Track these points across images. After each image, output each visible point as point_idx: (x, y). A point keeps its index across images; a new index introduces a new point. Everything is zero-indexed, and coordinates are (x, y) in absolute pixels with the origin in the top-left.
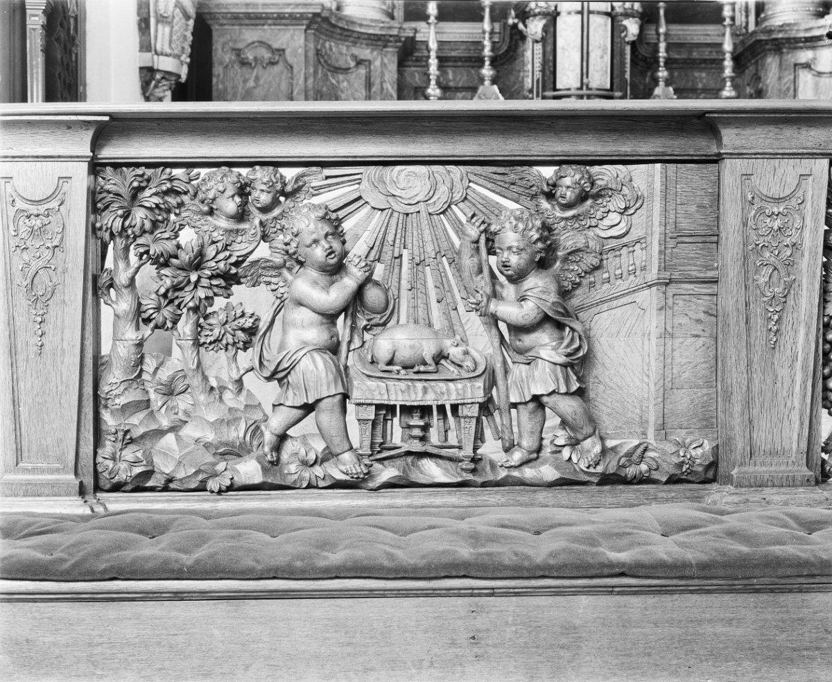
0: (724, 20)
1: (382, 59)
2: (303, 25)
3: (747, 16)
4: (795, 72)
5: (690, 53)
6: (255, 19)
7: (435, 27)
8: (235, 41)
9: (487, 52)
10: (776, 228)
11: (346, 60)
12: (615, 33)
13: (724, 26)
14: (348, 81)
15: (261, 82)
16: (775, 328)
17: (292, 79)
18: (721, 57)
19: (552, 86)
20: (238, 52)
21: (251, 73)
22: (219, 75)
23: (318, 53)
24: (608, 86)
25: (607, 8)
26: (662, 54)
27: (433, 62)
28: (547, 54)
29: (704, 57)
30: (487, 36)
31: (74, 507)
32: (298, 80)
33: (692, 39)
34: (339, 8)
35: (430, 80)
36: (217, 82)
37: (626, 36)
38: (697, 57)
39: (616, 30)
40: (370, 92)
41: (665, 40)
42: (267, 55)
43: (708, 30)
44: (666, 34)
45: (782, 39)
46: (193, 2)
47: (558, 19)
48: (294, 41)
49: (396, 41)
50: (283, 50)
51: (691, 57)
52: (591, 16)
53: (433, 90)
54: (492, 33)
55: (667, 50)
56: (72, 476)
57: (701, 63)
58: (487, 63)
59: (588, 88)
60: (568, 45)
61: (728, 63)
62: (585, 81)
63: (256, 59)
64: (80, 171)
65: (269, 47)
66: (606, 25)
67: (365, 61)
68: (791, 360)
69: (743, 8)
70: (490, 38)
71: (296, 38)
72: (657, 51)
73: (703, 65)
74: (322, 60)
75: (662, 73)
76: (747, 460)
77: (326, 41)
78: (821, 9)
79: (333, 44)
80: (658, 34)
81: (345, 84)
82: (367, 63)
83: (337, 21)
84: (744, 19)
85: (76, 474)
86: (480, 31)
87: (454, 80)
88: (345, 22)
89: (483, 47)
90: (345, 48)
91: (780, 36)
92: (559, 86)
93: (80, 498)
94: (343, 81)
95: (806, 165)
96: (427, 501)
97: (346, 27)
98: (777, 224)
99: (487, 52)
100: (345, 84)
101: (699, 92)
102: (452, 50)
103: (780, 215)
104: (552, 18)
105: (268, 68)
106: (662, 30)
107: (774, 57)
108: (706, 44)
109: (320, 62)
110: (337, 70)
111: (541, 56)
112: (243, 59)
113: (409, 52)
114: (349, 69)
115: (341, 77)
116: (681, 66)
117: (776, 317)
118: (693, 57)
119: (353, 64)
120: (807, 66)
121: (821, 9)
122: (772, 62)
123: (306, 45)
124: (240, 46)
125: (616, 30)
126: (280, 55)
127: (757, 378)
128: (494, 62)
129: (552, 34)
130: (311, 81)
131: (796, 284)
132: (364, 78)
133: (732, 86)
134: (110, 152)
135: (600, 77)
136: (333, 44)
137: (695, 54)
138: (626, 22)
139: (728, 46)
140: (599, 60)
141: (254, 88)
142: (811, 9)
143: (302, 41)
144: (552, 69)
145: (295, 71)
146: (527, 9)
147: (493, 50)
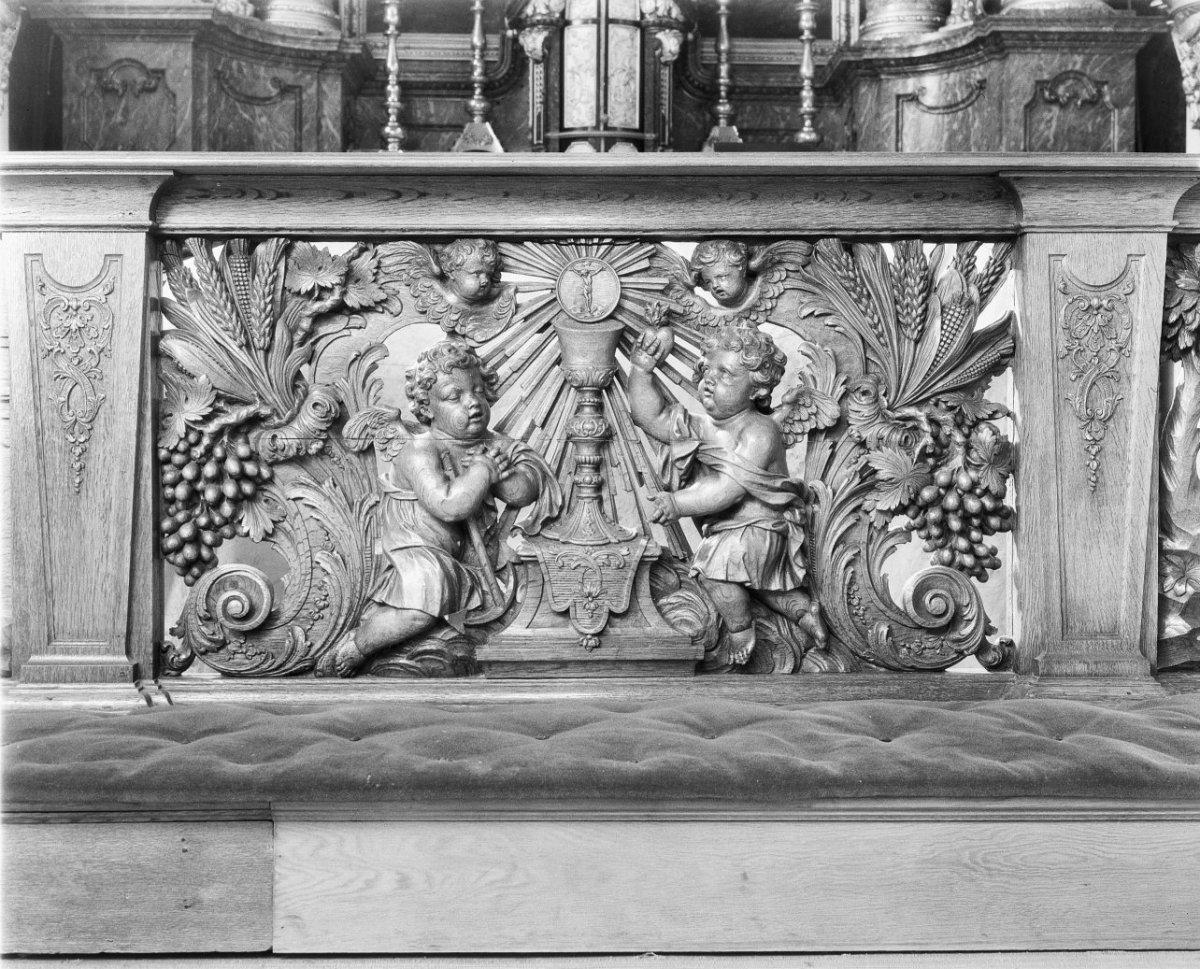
0: (801, 33)
1: (319, 85)
2: (189, 37)
3: (848, 28)
4: (897, 106)
5: (766, 79)
6: (129, 29)
7: (396, 39)
8: (94, 59)
9: (477, 74)
10: (74, 328)
11: (265, 87)
12: (646, 50)
13: (802, 41)
14: (270, 117)
15: (132, 116)
16: (78, 464)
17: (175, 111)
18: (796, 85)
19: (557, 124)
20: (100, 73)
21: (118, 104)
22: (72, 105)
23: (218, 76)
24: (637, 125)
25: (635, 16)
26: (724, 80)
27: (393, 89)
28: (552, 80)
29: (785, 85)
30: (477, 52)
31: (120, 699)
32: (184, 113)
33: (772, 60)
34: (260, 14)
35: (389, 115)
36: (69, 116)
37: (661, 55)
38: (776, 84)
39: (648, 45)
40: (301, 130)
41: (728, 60)
42: (141, 78)
43: (793, 47)
44: (729, 52)
45: (877, 60)
46: (8, 4)
47: (568, 33)
48: (176, 59)
49: (338, 61)
50: (163, 72)
51: (767, 85)
52: (610, 26)
53: (393, 130)
54: (484, 48)
55: (731, 74)
56: (124, 658)
57: (782, 93)
58: (478, 91)
59: (606, 128)
60: (580, 66)
61: (807, 94)
62: (602, 116)
63: (125, 84)
64: (136, 245)
65: (142, 67)
66: (632, 39)
67: (294, 87)
68: (102, 508)
69: (843, 17)
70: (482, 56)
71: (180, 55)
72: (717, 75)
73: (786, 96)
74: (226, 86)
75: (724, 108)
76: (44, 645)
77: (232, 59)
78: (939, 19)
79: (244, 64)
80: (718, 52)
81: (264, 119)
82: (297, 90)
83: (246, 31)
84: (843, 31)
85: (128, 653)
86: (469, 46)
87: (437, 114)
88: (257, 33)
89: (473, 68)
90: (263, 69)
91: (875, 55)
92: (567, 124)
93: (132, 685)
94: (260, 116)
95: (1133, 242)
96: (307, 697)
97: (260, 40)
98: (75, 323)
99: (477, 74)
100: (264, 119)
101: (781, 133)
102: (431, 72)
103: (1102, 310)
104: (558, 26)
105: (141, 98)
106: (724, 46)
107: (870, 86)
108: (790, 66)
109: (223, 89)
110: (251, 100)
111: (542, 82)
112: (105, 83)
113: (363, 76)
114: (269, 99)
115: (258, 110)
116: (752, 97)
117: (78, 451)
118: (770, 85)
119: (274, 92)
120: (914, 98)
121: (939, 19)
122: (865, 91)
123: (195, 65)
124: (102, 65)
125: (648, 48)
126: (159, 79)
127: (57, 532)
128: (489, 90)
129: (558, 51)
130: (204, 116)
131: (107, 405)
132: (292, 111)
133: (812, 126)
134: (179, 219)
135: (624, 112)
136: (244, 64)
137: (772, 80)
138: (660, 36)
139: (806, 70)
140: (622, 87)
141: (122, 124)
142: (924, 18)
143: (188, 60)
144: (557, 100)
145: (179, 101)
146: (523, 16)
147: (485, 73)
